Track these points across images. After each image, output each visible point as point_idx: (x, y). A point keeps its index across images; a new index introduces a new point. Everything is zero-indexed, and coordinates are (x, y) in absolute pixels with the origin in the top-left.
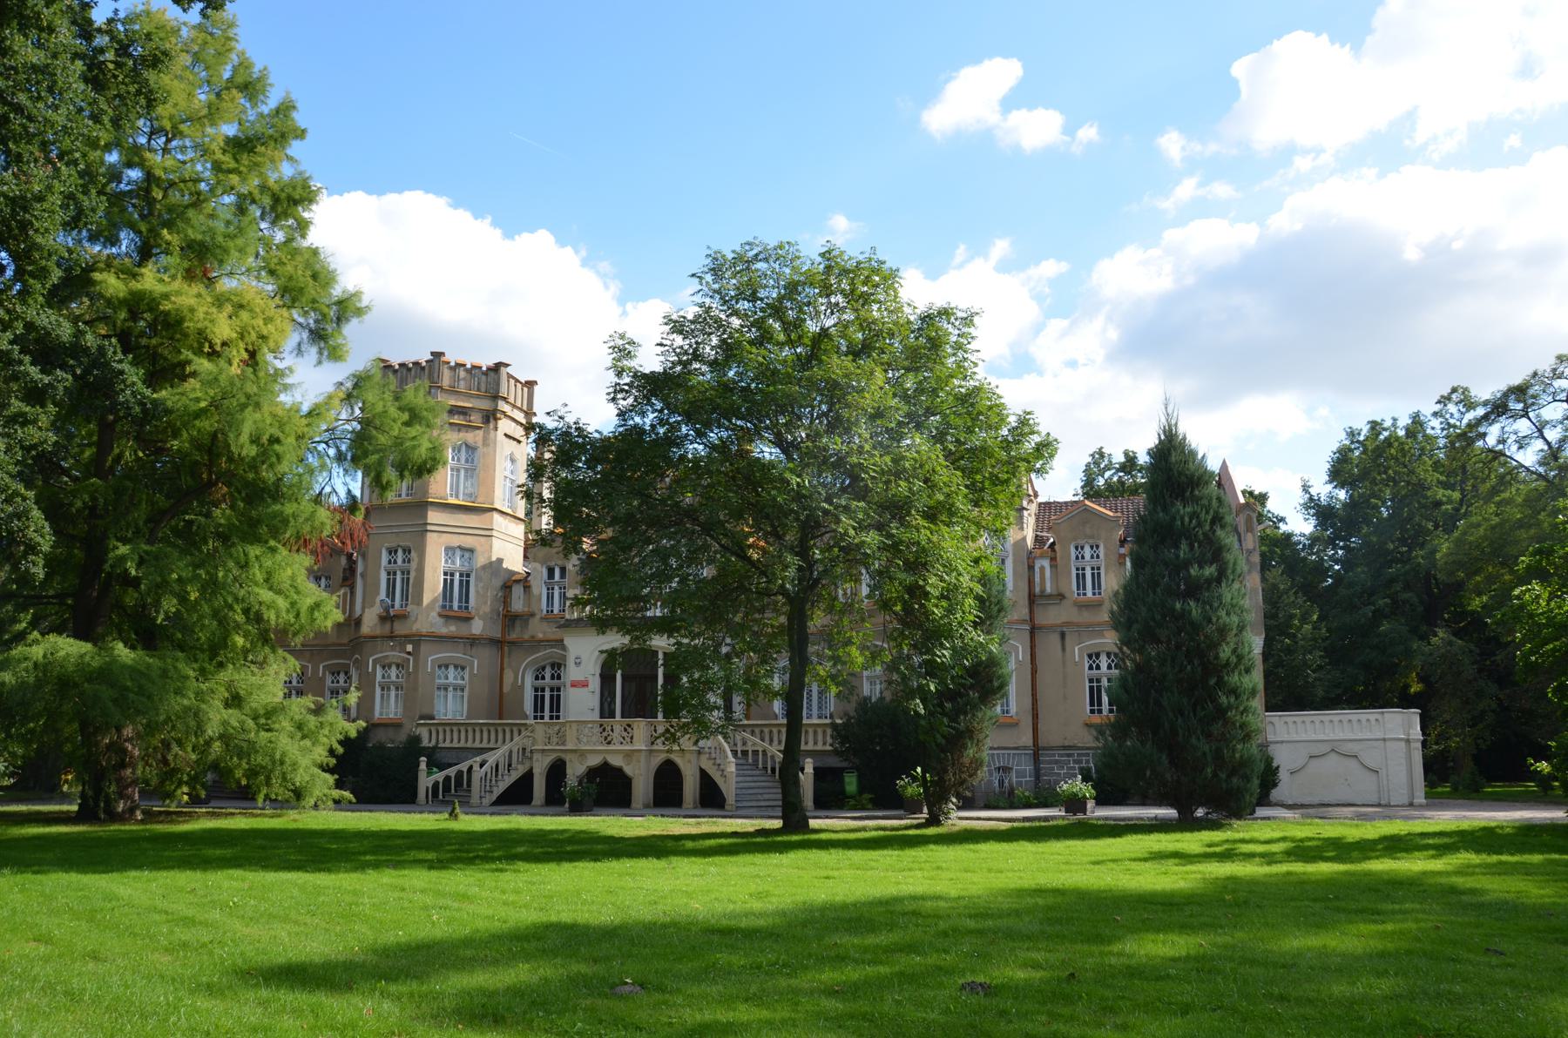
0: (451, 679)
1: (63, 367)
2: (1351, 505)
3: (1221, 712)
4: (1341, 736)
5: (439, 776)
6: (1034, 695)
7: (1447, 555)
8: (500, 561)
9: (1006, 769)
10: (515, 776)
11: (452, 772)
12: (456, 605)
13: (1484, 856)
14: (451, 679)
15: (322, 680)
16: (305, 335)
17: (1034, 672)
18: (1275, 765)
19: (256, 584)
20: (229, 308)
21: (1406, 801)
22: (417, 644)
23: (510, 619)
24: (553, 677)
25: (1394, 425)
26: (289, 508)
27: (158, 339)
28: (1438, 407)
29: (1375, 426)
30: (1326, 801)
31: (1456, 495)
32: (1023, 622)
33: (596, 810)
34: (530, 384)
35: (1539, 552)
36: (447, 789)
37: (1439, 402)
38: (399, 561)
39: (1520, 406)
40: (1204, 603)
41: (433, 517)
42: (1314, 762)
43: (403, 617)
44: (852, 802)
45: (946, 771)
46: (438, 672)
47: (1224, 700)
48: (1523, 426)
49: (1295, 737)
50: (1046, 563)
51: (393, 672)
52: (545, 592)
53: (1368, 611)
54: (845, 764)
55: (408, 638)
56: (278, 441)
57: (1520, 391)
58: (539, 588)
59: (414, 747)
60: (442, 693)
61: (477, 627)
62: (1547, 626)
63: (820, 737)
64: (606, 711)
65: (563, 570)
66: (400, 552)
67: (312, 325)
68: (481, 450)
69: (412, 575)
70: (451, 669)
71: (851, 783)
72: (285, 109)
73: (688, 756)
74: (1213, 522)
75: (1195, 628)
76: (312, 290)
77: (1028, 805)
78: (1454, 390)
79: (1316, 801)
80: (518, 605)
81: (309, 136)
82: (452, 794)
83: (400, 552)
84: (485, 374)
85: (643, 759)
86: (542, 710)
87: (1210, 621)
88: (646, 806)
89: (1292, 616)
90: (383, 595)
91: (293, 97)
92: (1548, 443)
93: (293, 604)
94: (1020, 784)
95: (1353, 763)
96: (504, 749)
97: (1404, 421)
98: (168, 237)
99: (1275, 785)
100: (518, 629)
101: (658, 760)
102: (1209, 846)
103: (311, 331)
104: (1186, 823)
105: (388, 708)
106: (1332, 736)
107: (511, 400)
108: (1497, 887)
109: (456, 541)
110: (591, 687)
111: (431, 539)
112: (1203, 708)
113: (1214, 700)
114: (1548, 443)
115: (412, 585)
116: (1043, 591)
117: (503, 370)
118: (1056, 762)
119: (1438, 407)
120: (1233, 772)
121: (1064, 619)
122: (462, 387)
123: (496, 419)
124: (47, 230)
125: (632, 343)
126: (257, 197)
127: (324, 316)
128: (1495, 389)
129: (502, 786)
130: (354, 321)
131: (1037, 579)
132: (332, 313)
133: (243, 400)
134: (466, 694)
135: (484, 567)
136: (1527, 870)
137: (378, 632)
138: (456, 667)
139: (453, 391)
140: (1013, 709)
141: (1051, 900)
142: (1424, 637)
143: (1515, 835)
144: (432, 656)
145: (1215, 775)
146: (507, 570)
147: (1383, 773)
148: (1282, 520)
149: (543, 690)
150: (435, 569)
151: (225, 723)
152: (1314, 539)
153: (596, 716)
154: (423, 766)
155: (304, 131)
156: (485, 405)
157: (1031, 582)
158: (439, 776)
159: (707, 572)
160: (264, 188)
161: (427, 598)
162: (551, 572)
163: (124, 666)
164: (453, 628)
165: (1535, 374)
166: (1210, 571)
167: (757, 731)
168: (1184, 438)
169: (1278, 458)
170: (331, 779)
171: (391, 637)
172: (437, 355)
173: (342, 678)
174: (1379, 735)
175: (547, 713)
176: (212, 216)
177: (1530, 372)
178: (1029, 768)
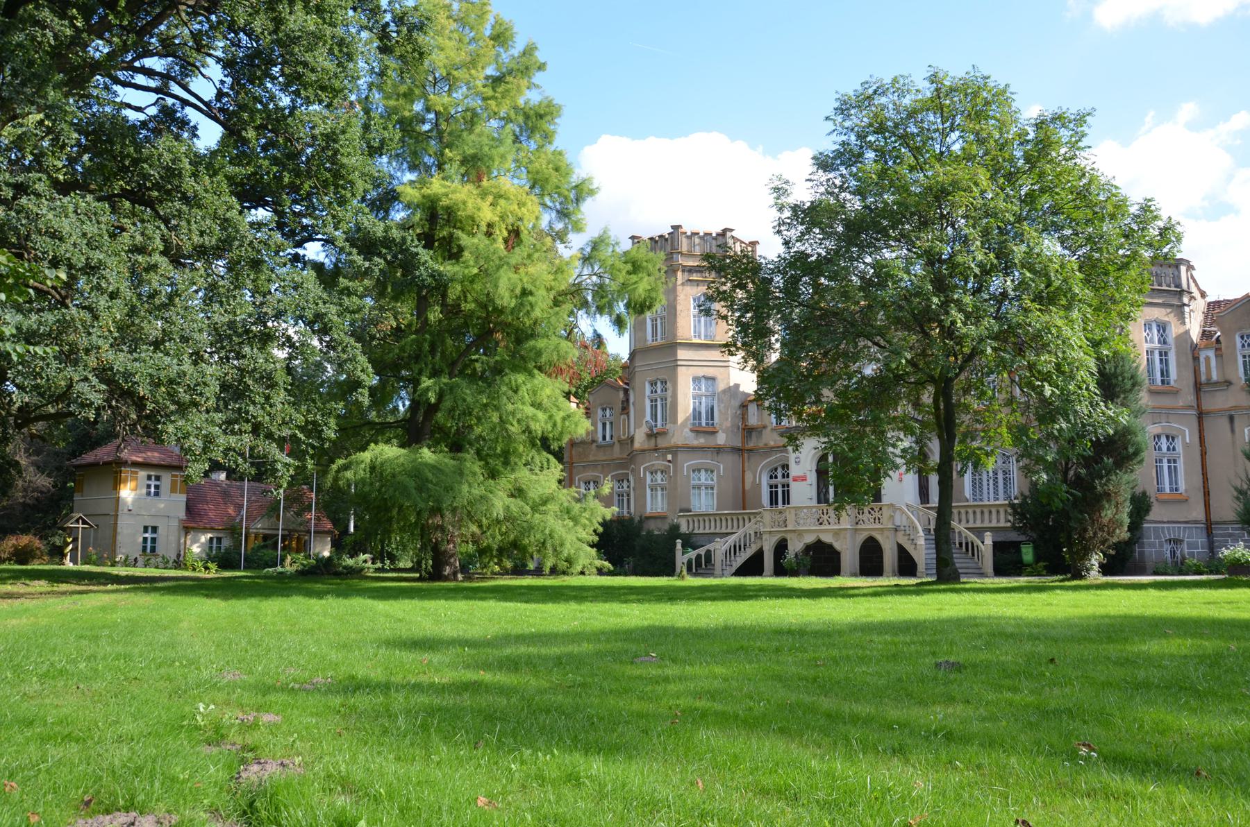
0: (703, 481)
1: (380, 255)
5: (692, 554)
6: (1204, 474)
8: (737, 386)
9: (1177, 542)
10: (749, 553)
11: (702, 551)
14: (703, 481)
16: (554, 214)
17: (1203, 454)
19: (523, 403)
20: (490, 198)
22: (675, 454)
26: (541, 343)
27: (439, 225)
32: (1191, 407)
36: (699, 564)
38: (659, 391)
41: (682, 354)
43: (663, 433)
44: (1029, 569)
45: (1085, 530)
50: (1211, 354)
51: (659, 476)
55: (668, 450)
56: (531, 293)
59: (674, 532)
60: (697, 491)
61: (721, 439)
63: (971, 516)
64: (822, 497)
66: (659, 384)
67: (558, 207)
69: (669, 400)
70: (703, 472)
71: (1028, 554)
72: (529, 51)
73: (886, 533)
76: (554, 179)
81: (548, 67)
83: (659, 384)
84: (715, 239)
85: (848, 535)
90: (648, 418)
93: (551, 417)
94: (1192, 555)
96: (741, 532)
98: (450, 155)
101: (861, 538)
103: (558, 212)
105: (655, 504)
109: (701, 372)
110: (809, 482)
111: (681, 371)
115: (670, 409)
116: (1209, 379)
117: (729, 234)
118: (1230, 535)
121: (1231, 403)
124: (349, 154)
125: (787, 182)
126: (513, 116)
127: (566, 198)
130: (589, 200)
131: (1203, 368)
132: (572, 195)
133: (497, 262)
135: (724, 391)
137: (646, 447)
138: (706, 470)
140: (1182, 486)
146: (744, 393)
149: (776, 487)
151: (507, 508)
153: (814, 503)
154: (679, 546)
155: (544, 64)
157: (1196, 372)
158: (692, 554)
159: (869, 370)
160: (515, 108)
161: (681, 418)
163: (426, 464)
170: (593, 551)
171: (656, 450)
172: (676, 228)
173: (625, 484)
176: (480, 135)
178: (1201, 540)
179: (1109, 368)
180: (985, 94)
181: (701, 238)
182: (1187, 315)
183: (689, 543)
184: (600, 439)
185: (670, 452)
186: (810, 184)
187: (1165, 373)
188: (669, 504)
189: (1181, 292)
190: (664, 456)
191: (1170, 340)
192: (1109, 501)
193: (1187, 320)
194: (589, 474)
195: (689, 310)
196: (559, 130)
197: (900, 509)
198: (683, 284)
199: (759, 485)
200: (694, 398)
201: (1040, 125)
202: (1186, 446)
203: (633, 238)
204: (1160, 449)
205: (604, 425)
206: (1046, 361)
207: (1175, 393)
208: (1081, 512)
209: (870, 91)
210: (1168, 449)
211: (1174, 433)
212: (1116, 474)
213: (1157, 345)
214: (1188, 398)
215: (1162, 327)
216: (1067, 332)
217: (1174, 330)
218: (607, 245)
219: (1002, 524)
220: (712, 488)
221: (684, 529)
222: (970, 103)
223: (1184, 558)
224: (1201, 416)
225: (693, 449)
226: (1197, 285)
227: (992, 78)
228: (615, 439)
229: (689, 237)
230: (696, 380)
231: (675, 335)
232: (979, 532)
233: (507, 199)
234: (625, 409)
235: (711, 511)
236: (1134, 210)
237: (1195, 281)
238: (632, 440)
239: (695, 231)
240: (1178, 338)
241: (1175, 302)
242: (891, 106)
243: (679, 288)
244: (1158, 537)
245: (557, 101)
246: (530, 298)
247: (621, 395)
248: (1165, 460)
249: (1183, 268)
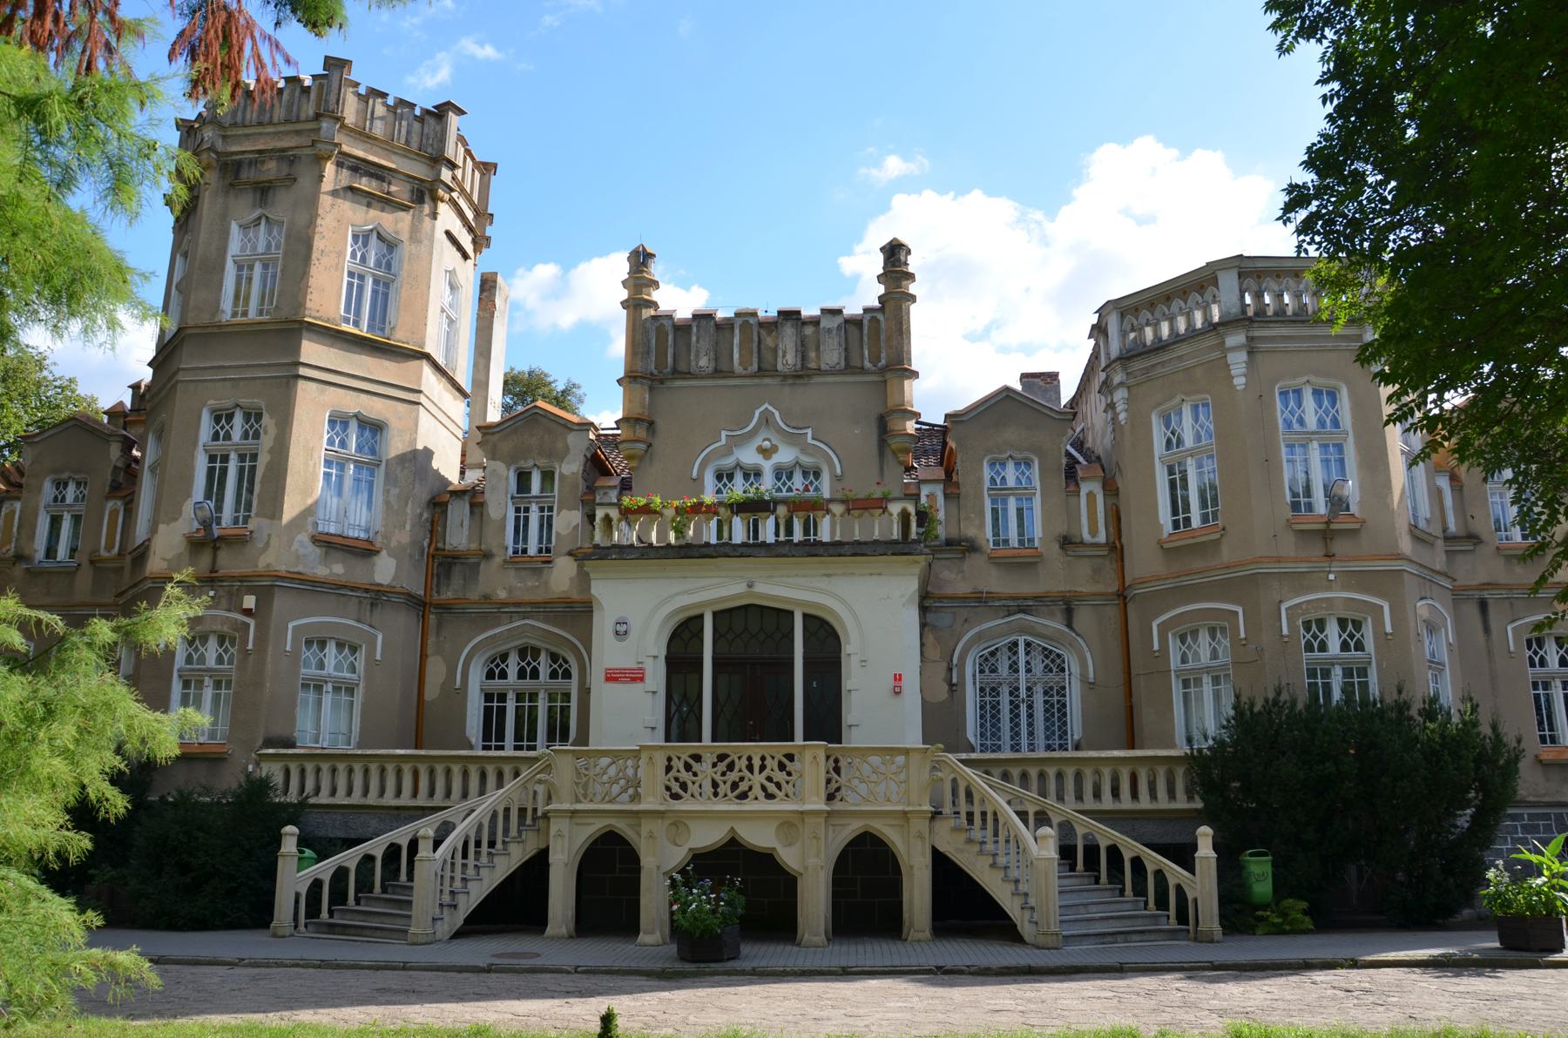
5: (324, 869)
10: (1011, 906)
11: (349, 858)
14: (330, 669)
23: (443, 563)
24: (522, 674)
34: (487, 169)
38: (236, 435)
41: (312, 351)
43: (239, 541)
46: (306, 654)
52: (511, 514)
55: (248, 582)
58: (500, 507)
60: (311, 696)
61: (384, 570)
64: (681, 722)
65: (548, 476)
66: (238, 420)
68: (407, 248)
69: (263, 460)
70: (331, 649)
80: (458, 536)
83: (238, 420)
100: (457, 580)
109: (353, 404)
117: (453, 120)
121: (1482, 577)
122: (379, 129)
123: (435, 199)
129: (478, 892)
134: (358, 698)
138: (340, 646)
139: (362, 135)
141: (730, 965)
144: (295, 621)
149: (502, 697)
150: (310, 452)
156: (419, 170)
158: (324, 869)
162: (523, 479)
164: (338, 569)
184: (40, 554)
185: (250, 591)
188: (235, 723)
195: (341, 254)
198: (334, 193)
200: (328, 463)
205: (55, 522)
220: (350, 691)
228: (82, 557)
230: (339, 421)
231: (300, 305)
235: (343, 748)
243: (325, 200)
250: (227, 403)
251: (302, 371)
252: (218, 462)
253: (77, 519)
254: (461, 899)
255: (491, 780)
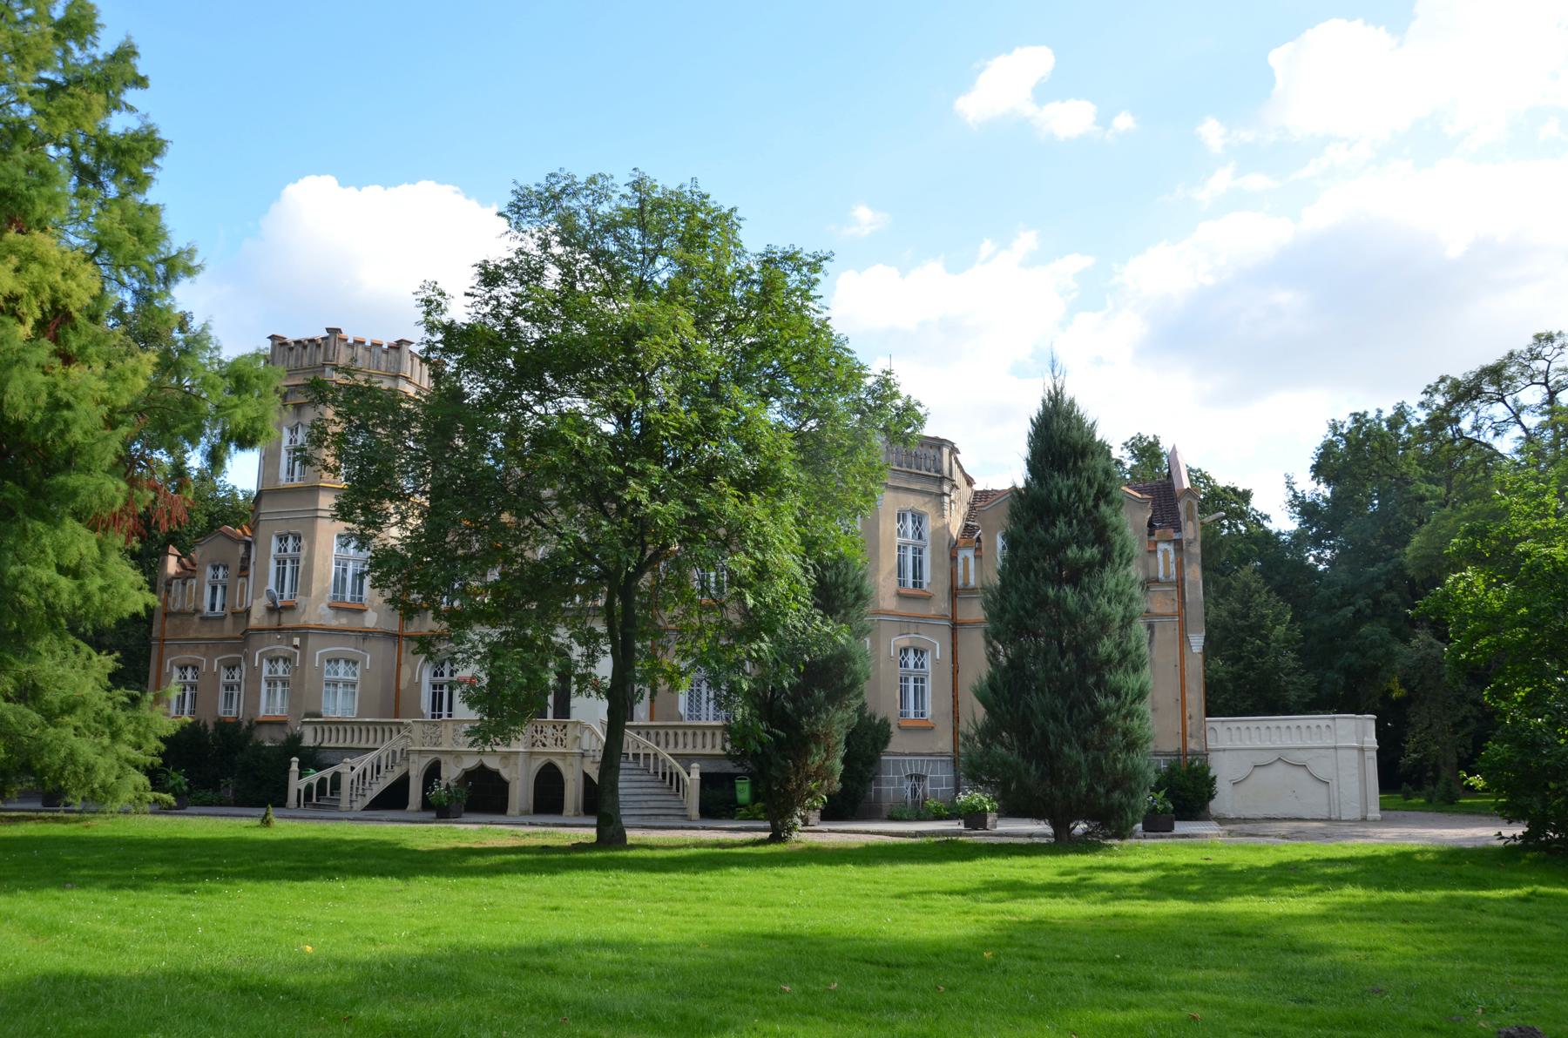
0: (341, 675)
2: (1335, 501)
3: (1099, 716)
4: (1289, 744)
5: (313, 777)
7: (1417, 549)
9: (919, 778)
11: (327, 773)
12: (348, 598)
13: (1372, 892)
15: (217, 675)
17: (955, 672)
18: (1212, 774)
21: (1359, 817)
25: (1378, 417)
26: (74, 480)
28: (1424, 398)
29: (1358, 418)
30: (1272, 814)
31: (1441, 490)
32: (943, 617)
33: (466, 817)
35: (1470, 532)
36: (308, 796)
37: (1426, 392)
39: (1492, 389)
40: (1082, 589)
42: (1260, 773)
43: (290, 608)
44: (744, 811)
45: (788, 780)
47: (1102, 702)
48: (1499, 411)
49: (1239, 745)
50: (970, 554)
51: (281, 666)
53: (1348, 612)
54: (739, 770)
57: (1495, 373)
59: (293, 745)
60: (331, 689)
61: (371, 620)
62: (1474, 617)
63: (681, 740)
66: (290, 539)
70: (342, 664)
71: (743, 792)
72: (125, 54)
73: (569, 759)
74: (1097, 499)
75: (1072, 619)
77: (939, 817)
78: (1443, 380)
79: (1260, 814)
82: (323, 798)
83: (290, 539)
84: (386, 352)
86: (440, 709)
87: (1087, 610)
88: (525, 813)
89: (1264, 616)
90: (272, 585)
91: (135, 41)
92: (1526, 430)
94: (934, 793)
95: (1301, 773)
97: (1388, 412)
99: (1211, 797)
102: (1063, 874)
104: (1063, 843)
105: (271, 704)
106: (1278, 744)
107: (416, 380)
108: (1348, 938)
112: (1080, 712)
113: (1093, 703)
114: (1526, 430)
116: (966, 583)
119: (1424, 398)
120: (1117, 784)
125: (442, 294)
128: (1467, 370)
129: (377, 789)
136: (1402, 915)
137: (265, 625)
138: (347, 662)
140: (929, 711)
142: (1406, 641)
143: (1434, 862)
144: (319, 651)
145: (1091, 789)
147: (1334, 784)
148: (1266, 517)
149: (441, 687)
152: (1297, 536)
154: (295, 767)
161: (316, 588)
165: (1511, 354)
166: (1091, 553)
167: (652, 732)
168: (1072, 403)
169: (1265, 457)
171: (279, 630)
174: (1330, 742)
175: (445, 711)
177: (1506, 353)
179: (830, 575)
180: (701, 216)
181: (368, 349)
182: (947, 507)
183: (312, 760)
184: (207, 608)
186: (470, 300)
187: (918, 574)
188: (291, 706)
189: (941, 480)
190: (290, 639)
191: (927, 534)
192: (817, 743)
193: (947, 513)
194: (187, 657)
196: (157, 175)
197: (589, 728)
199: (419, 684)
201: (768, 261)
202: (935, 662)
203: (272, 337)
204: (906, 665)
205: (214, 589)
206: (740, 563)
207: (927, 598)
208: (785, 758)
209: (558, 189)
210: (916, 666)
211: (922, 646)
212: (827, 711)
213: (910, 539)
214: (941, 605)
215: (918, 518)
216: (769, 528)
217: (929, 525)
218: (205, 348)
219: (718, 751)
220: (353, 686)
221: (308, 740)
222: (687, 224)
223: (925, 796)
224: (955, 626)
225: (330, 631)
226: (962, 470)
227: (711, 199)
228: (227, 611)
229: (351, 346)
232: (686, 760)
233: (44, 265)
234: (244, 570)
236: (869, 381)
237: (960, 466)
238: (248, 612)
239: (360, 336)
240: (935, 533)
241: (934, 489)
242: (583, 212)
244: (897, 772)
245: (163, 135)
246: (65, 413)
247: (242, 549)
248: (911, 679)
249: (946, 451)
250: (283, 532)
251: (320, 513)
252: (281, 562)
253: (224, 588)
254: (368, 793)
255: (387, 734)
